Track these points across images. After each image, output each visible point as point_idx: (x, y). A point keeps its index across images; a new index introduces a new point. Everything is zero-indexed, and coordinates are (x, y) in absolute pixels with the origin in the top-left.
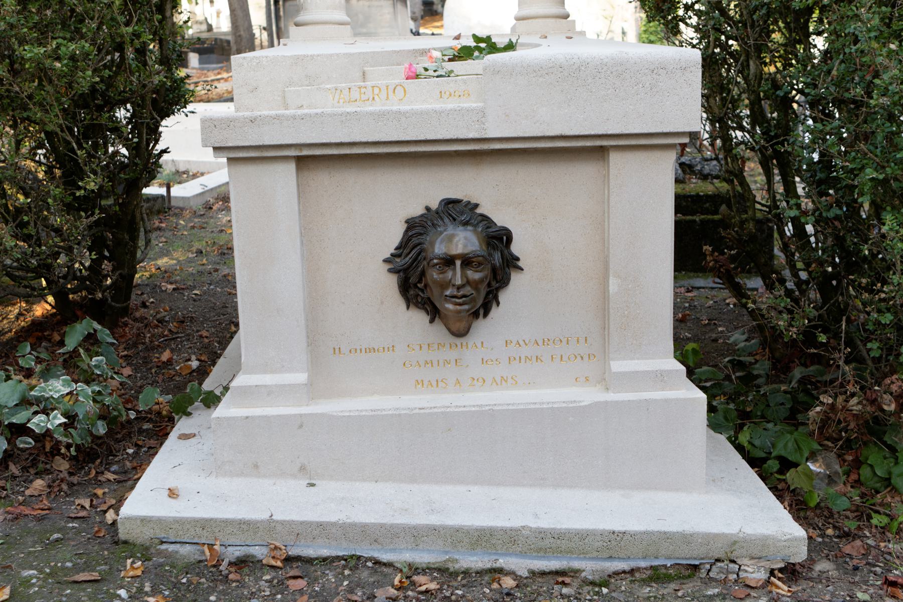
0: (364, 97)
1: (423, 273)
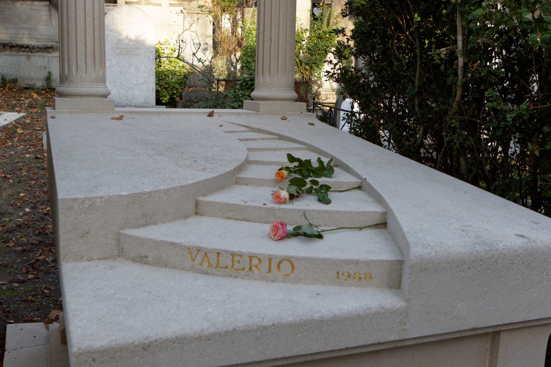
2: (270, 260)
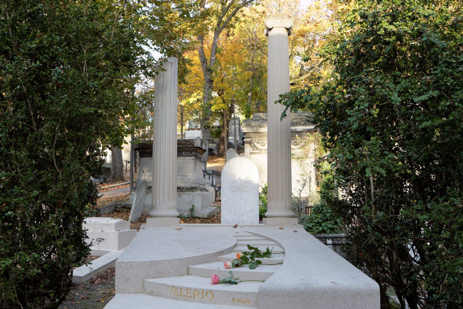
0: (189, 295)
2: (203, 291)
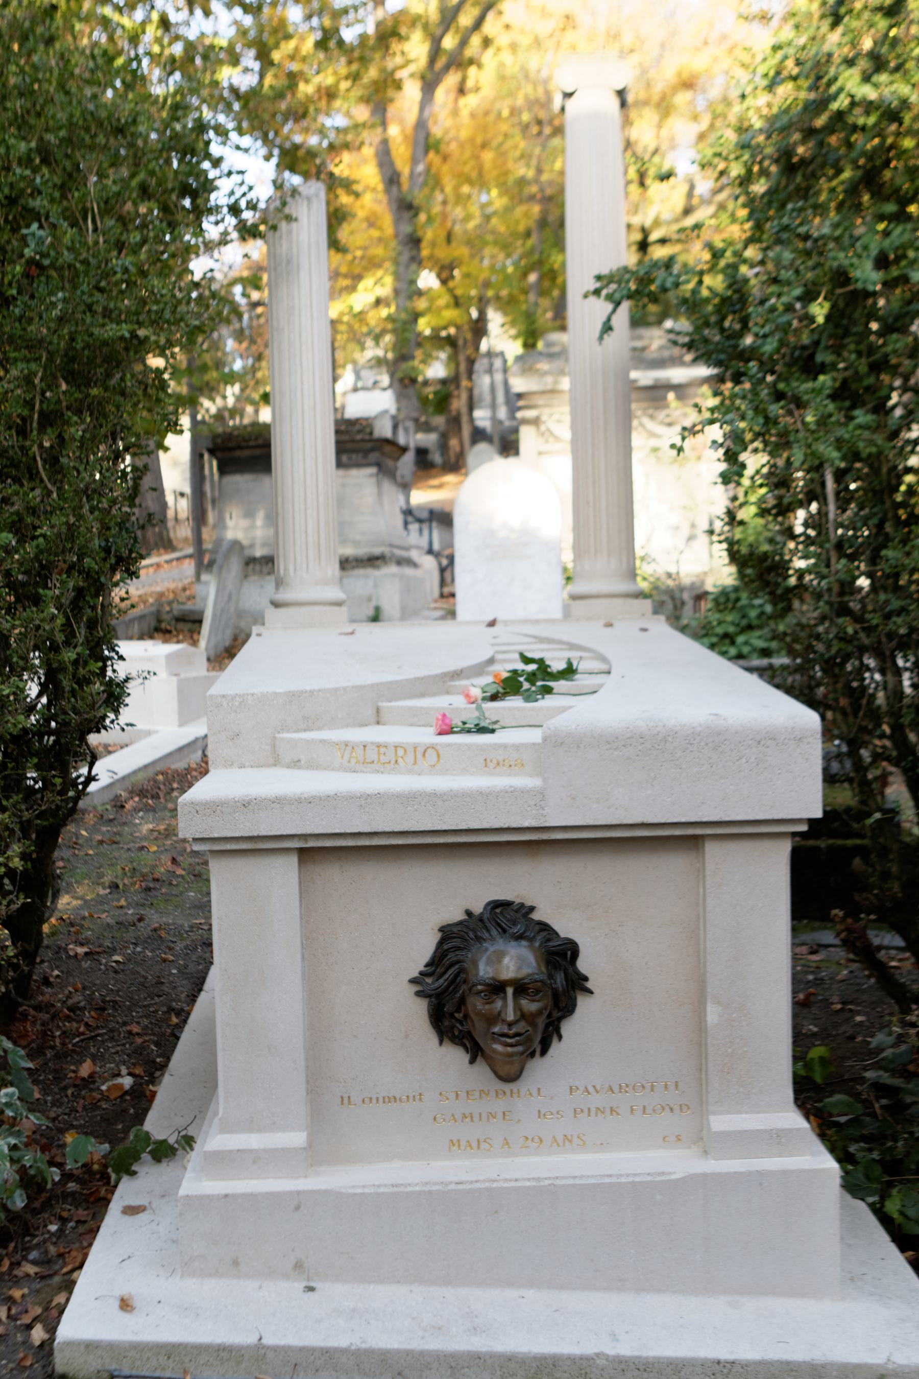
0: (384, 759)
1: (462, 1001)
